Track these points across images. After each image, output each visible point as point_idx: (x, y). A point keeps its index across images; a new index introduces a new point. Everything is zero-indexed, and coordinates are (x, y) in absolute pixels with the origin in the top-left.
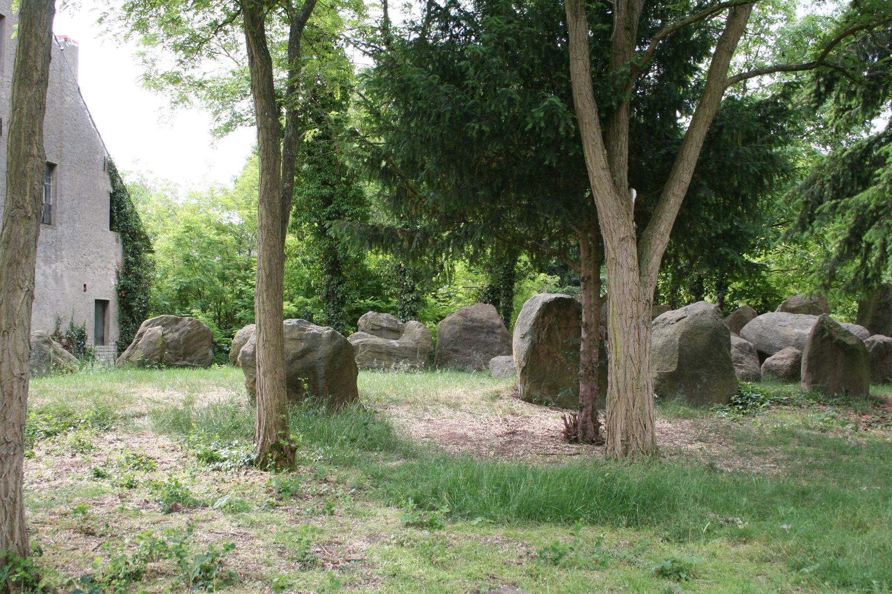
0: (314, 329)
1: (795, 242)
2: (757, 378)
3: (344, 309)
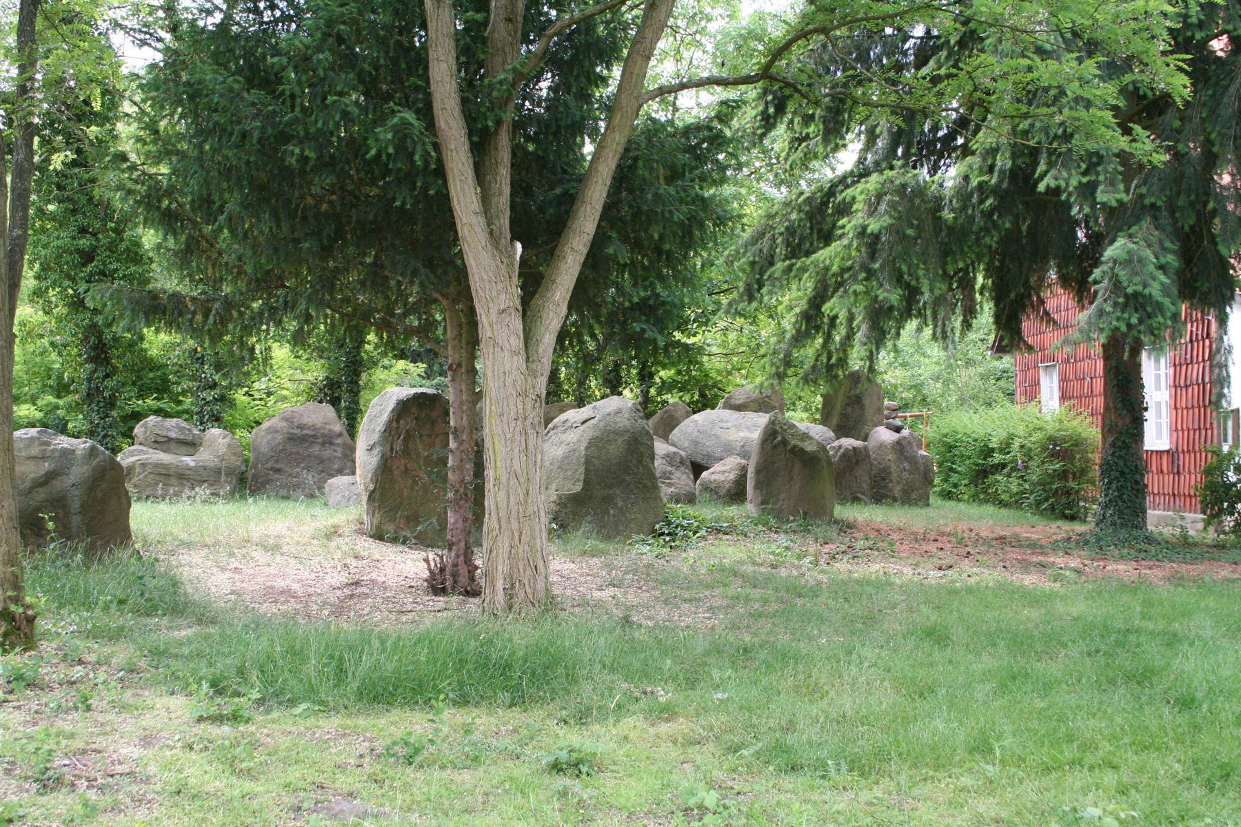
0: (64, 442)
1: (741, 315)
2: (691, 499)
3: (114, 413)
